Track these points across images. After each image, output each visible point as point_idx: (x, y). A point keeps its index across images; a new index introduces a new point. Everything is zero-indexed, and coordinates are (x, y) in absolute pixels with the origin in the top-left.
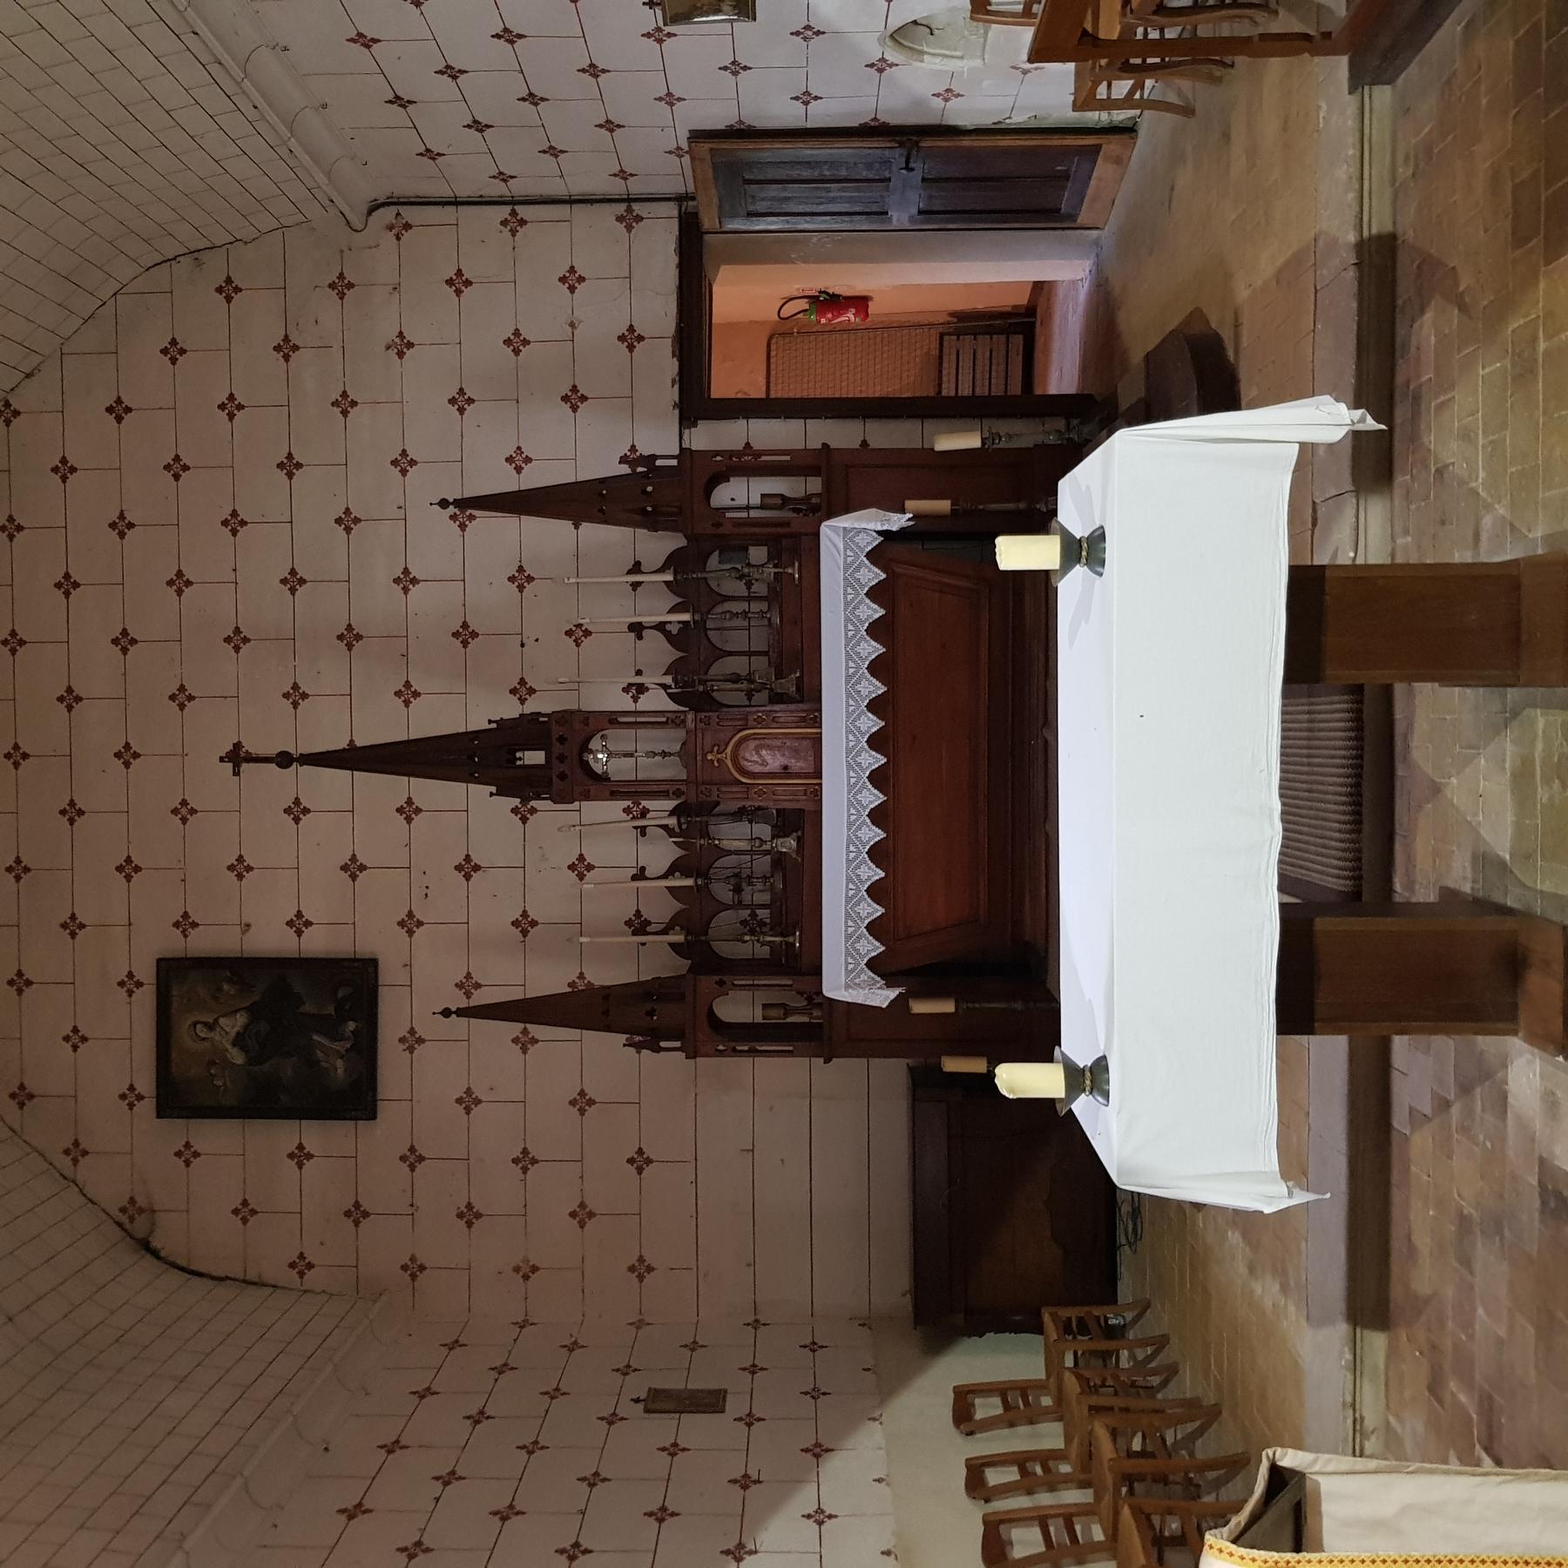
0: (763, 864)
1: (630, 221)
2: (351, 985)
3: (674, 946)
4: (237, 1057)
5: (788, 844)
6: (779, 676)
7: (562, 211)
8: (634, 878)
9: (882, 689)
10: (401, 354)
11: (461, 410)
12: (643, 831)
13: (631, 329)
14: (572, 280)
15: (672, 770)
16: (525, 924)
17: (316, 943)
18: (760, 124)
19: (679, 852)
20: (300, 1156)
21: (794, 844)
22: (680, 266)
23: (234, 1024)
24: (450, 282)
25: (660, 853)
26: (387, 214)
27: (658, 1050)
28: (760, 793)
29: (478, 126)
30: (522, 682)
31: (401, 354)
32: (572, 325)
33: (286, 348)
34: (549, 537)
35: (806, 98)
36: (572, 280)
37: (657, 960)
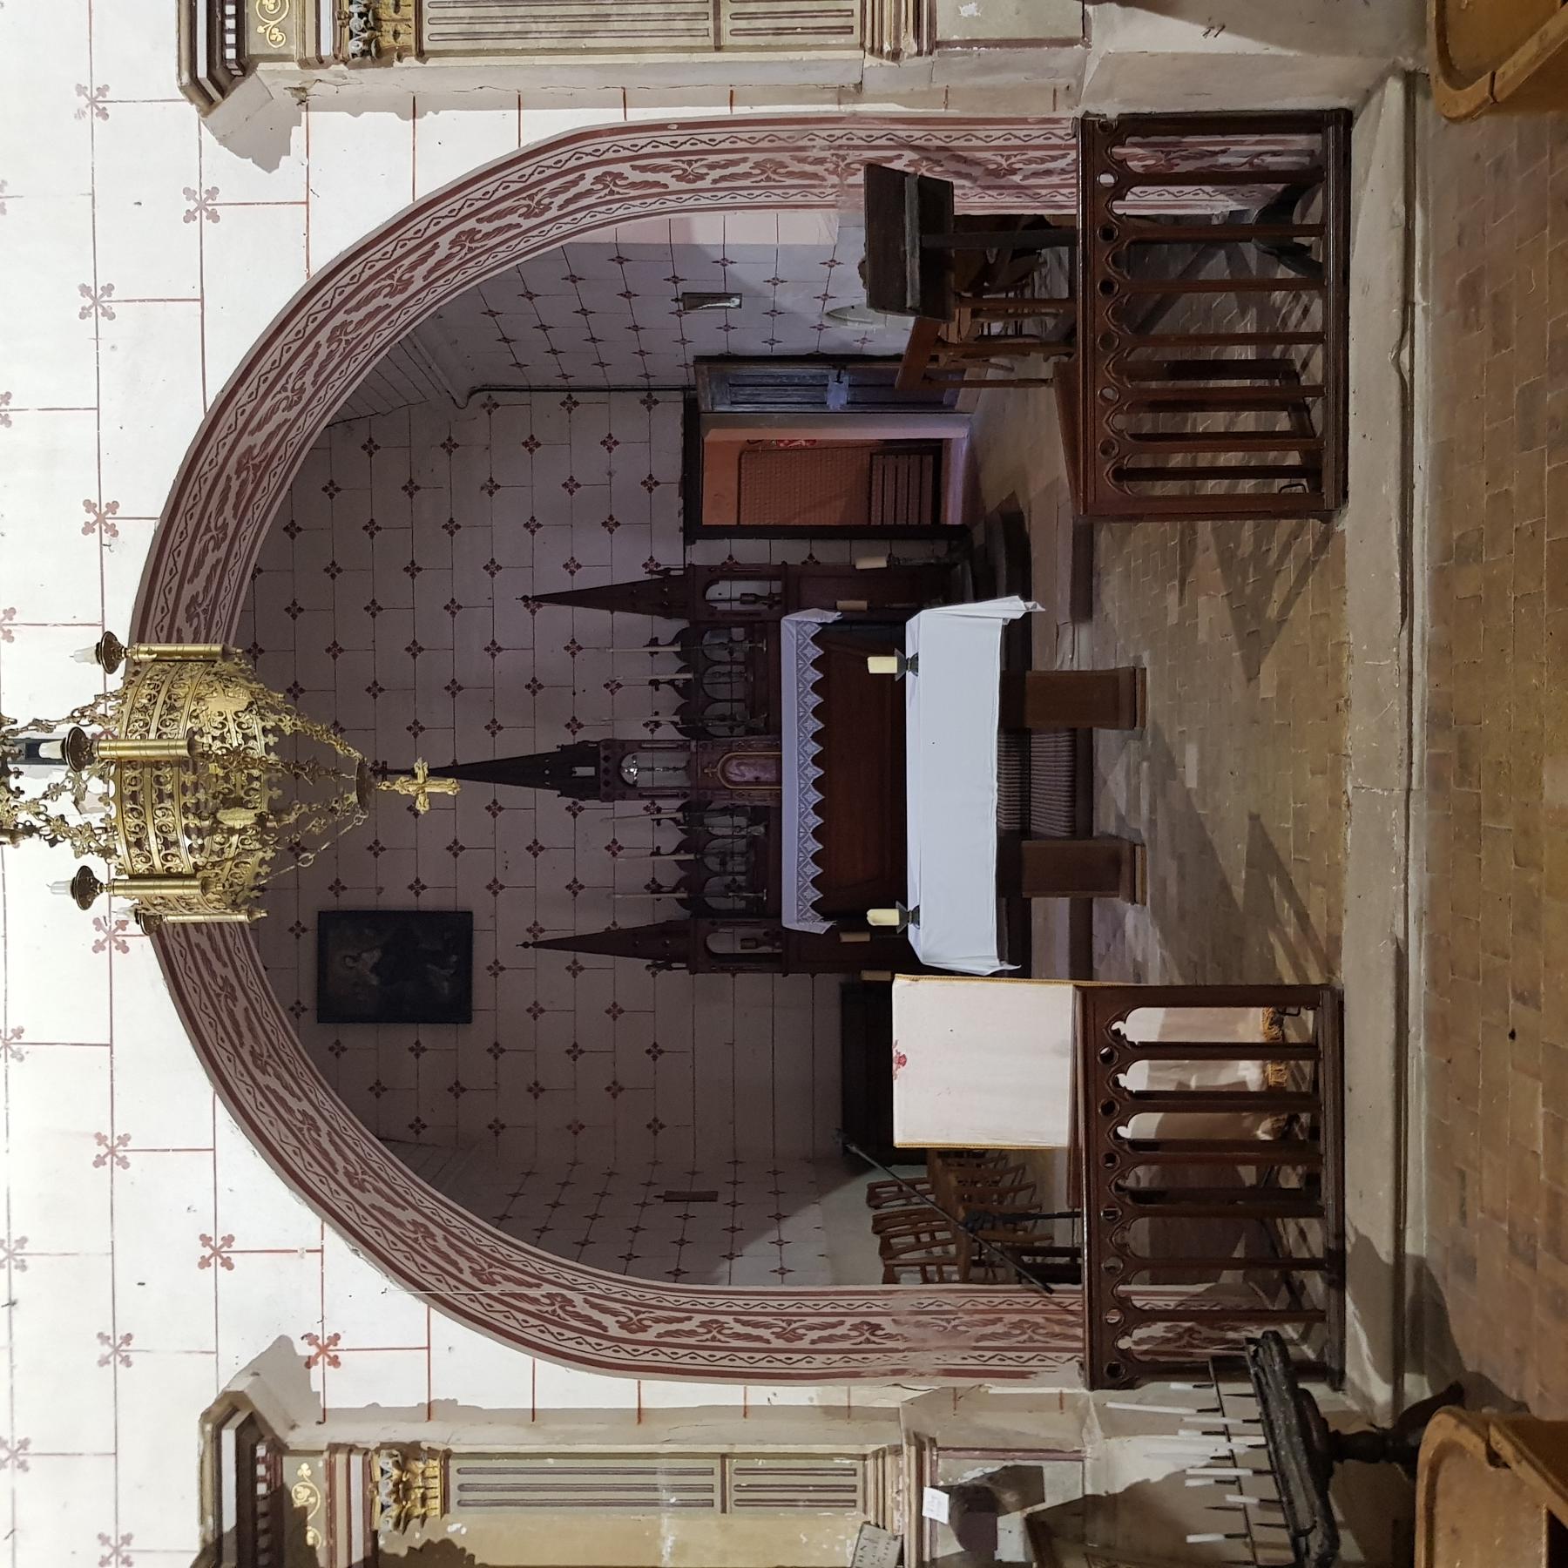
0: (741, 844)
1: (650, 403)
2: (451, 932)
4: (375, 981)
5: (760, 830)
7: (602, 396)
8: (653, 854)
10: (491, 493)
14: (609, 443)
15: (678, 780)
16: (575, 887)
17: (429, 901)
19: (681, 837)
20: (418, 1049)
21: (762, 829)
22: (685, 434)
23: (371, 957)
24: (525, 444)
25: (671, 838)
27: (671, 969)
31: (491, 493)
32: (610, 474)
33: (411, 488)
34: (598, 618)
36: (609, 443)
37: (669, 909)
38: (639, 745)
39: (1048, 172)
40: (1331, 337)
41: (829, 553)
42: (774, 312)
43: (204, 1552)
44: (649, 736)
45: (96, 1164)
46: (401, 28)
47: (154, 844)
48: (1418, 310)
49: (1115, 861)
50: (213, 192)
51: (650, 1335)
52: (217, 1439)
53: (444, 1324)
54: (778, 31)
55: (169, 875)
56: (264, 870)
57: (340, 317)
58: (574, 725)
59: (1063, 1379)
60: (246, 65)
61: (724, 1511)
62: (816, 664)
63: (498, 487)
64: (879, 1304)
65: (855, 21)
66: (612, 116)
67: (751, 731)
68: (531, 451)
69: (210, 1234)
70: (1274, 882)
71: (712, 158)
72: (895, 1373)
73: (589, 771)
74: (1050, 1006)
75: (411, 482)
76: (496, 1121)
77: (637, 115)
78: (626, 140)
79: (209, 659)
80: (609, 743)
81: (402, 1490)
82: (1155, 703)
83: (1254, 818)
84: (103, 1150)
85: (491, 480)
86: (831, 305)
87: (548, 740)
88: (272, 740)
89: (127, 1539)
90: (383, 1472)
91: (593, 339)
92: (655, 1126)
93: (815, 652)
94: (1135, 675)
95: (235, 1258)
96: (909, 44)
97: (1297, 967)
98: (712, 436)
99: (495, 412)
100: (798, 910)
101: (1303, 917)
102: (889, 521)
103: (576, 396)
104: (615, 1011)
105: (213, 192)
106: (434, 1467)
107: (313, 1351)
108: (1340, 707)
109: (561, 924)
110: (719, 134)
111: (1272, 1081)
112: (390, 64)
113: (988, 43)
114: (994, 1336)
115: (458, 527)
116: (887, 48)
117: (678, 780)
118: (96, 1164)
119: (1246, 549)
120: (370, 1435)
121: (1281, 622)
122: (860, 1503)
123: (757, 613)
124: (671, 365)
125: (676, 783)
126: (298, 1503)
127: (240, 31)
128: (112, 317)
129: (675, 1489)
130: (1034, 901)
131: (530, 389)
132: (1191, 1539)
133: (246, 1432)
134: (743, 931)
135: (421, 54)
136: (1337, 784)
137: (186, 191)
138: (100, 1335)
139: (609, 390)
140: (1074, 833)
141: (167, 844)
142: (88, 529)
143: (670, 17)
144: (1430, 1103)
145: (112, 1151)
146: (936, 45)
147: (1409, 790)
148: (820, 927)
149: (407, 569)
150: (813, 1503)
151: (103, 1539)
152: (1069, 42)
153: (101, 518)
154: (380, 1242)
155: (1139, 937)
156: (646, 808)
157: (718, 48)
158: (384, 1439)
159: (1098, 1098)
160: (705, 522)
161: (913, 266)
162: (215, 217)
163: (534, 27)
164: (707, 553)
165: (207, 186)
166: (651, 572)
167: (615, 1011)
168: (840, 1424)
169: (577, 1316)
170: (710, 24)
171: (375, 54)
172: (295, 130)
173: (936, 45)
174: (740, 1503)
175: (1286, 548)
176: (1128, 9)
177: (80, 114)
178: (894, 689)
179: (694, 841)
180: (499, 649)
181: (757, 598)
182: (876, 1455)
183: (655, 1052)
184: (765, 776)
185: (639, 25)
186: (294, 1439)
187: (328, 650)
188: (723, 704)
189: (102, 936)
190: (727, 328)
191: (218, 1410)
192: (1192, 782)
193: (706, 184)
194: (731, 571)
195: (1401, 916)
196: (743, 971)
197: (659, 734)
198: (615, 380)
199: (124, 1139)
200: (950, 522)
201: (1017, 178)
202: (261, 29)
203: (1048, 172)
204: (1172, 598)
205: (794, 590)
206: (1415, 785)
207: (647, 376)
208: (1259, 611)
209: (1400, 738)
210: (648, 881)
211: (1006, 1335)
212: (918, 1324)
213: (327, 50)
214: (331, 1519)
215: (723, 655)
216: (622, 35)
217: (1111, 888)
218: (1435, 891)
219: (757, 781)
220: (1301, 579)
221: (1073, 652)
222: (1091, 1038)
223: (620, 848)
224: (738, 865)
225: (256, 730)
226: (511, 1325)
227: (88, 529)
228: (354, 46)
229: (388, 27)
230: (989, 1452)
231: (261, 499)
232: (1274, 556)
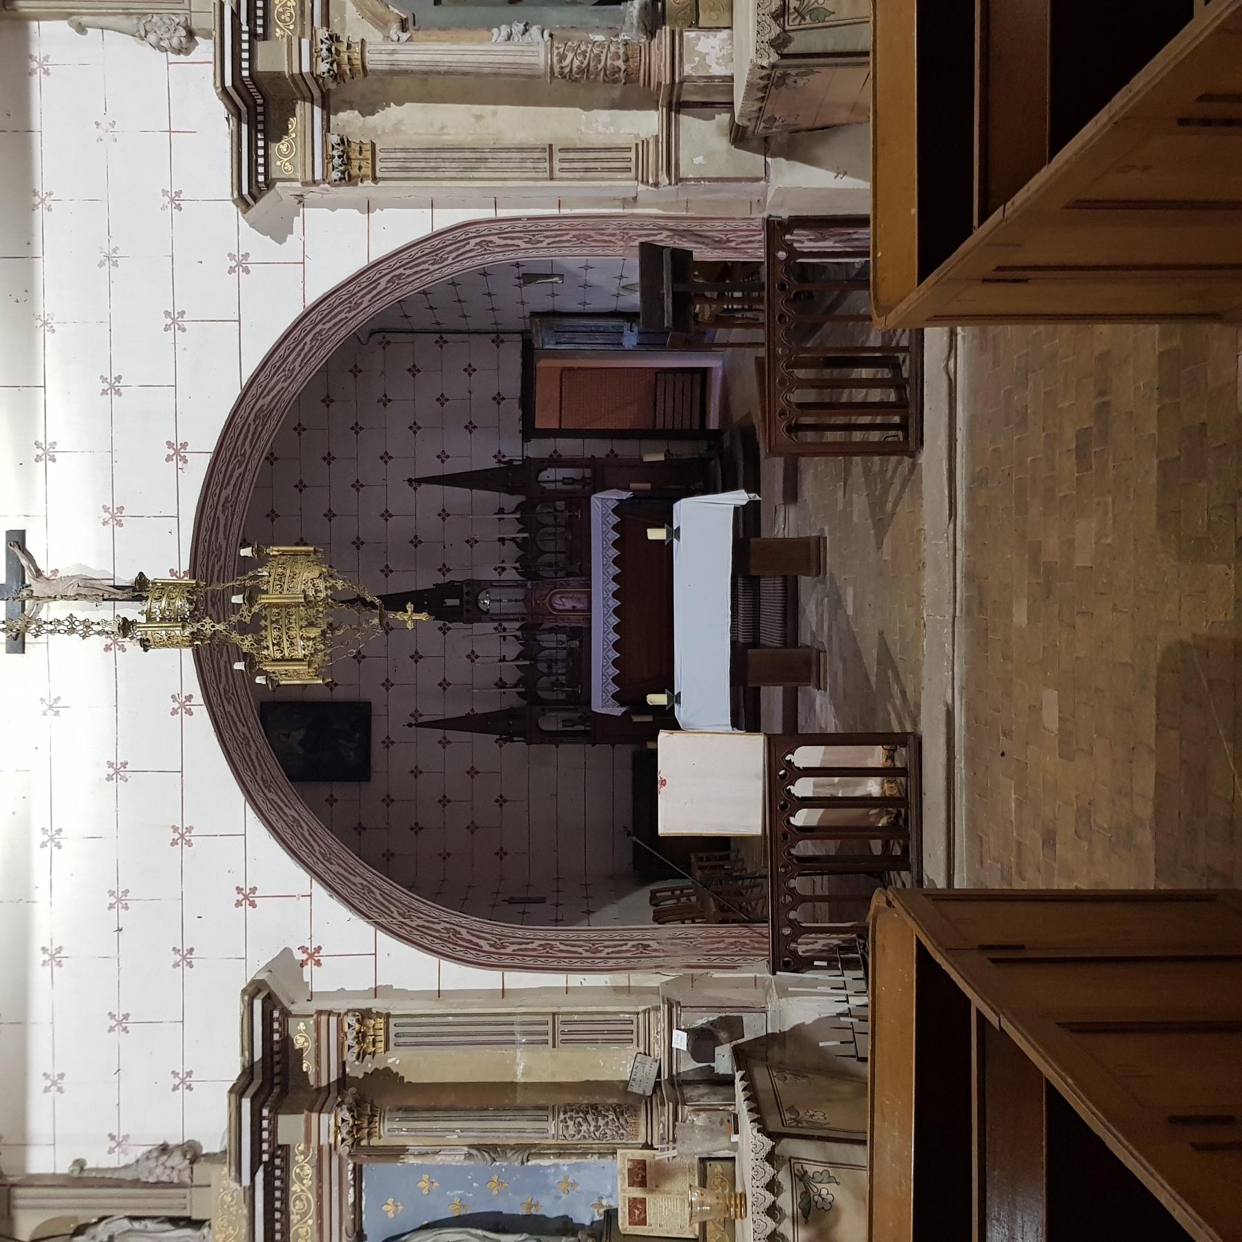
1: (498, 342)
3: (518, 693)
4: (300, 751)
6: (571, 564)
8: (500, 661)
10: (385, 405)
12: (504, 638)
14: (470, 370)
15: (519, 608)
16: (444, 685)
19: (520, 648)
22: (523, 364)
23: (298, 735)
26: (379, 337)
28: (563, 620)
30: (444, 565)
31: (385, 405)
34: (459, 495)
36: (470, 370)
37: (511, 699)
38: (491, 584)
39: (751, 242)
40: (913, 349)
41: (625, 449)
42: (585, 286)
43: (243, 1073)
44: (498, 578)
46: (363, 164)
47: (286, 644)
48: (959, 338)
49: (807, 663)
50: (246, 256)
51: (509, 950)
52: (251, 1005)
53: (383, 937)
54: (587, 170)
55: (292, 660)
56: (327, 658)
57: (320, 327)
58: (444, 569)
59: (758, 970)
60: (269, 184)
61: (554, 1046)
62: (615, 528)
64: (650, 934)
65: (632, 165)
66: (489, 213)
67: (569, 575)
69: (242, 886)
70: (890, 672)
71: (546, 233)
72: (656, 967)
73: (456, 602)
74: (753, 747)
75: (328, 396)
76: (388, 851)
77: (503, 213)
78: (497, 226)
79: (307, 554)
80: (470, 582)
81: (361, 1037)
82: (831, 560)
83: (881, 634)
84: (177, 836)
85: (385, 396)
86: (624, 282)
87: (427, 580)
88: (329, 592)
89: (190, 1074)
90: (350, 1026)
91: (459, 301)
92: (501, 854)
93: (615, 519)
94: (820, 541)
95: (257, 901)
96: (663, 178)
97: (901, 723)
98: (542, 364)
99: (388, 348)
100: (603, 701)
101: (903, 693)
102: (669, 426)
104: (473, 772)
105: (246, 256)
106: (380, 1023)
107: (305, 957)
108: (921, 566)
109: (435, 709)
110: (552, 223)
111: (888, 793)
112: (356, 184)
113: (710, 180)
114: (718, 949)
115: (361, 428)
116: (651, 181)
117: (519, 608)
119: (876, 468)
120: (341, 1006)
121: (893, 515)
122: (635, 1041)
123: (574, 492)
124: (513, 317)
125: (517, 611)
126: (297, 1047)
127: (266, 165)
128: (184, 330)
129: (524, 1033)
130: (764, 689)
131: (413, 332)
132: (821, 1044)
133: (267, 1002)
134: (566, 715)
135: (375, 179)
136: (919, 613)
137: (230, 255)
138: (174, 949)
139: (469, 332)
140: (785, 644)
141: (292, 644)
142: (169, 459)
143: (523, 160)
144: (967, 800)
145: (182, 836)
146: (679, 180)
147: (954, 617)
148: (618, 711)
149: (324, 459)
151: (175, 1074)
152: (757, 180)
153: (177, 452)
154: (345, 892)
155: (822, 710)
156: (496, 629)
157: (552, 179)
158: (350, 1007)
159: (779, 800)
160: (537, 426)
161: (668, 302)
162: (247, 271)
163: (442, 165)
164: (539, 449)
165: (242, 252)
166: (499, 461)
167: (473, 772)
168: (623, 997)
169: (464, 940)
170: (547, 165)
171: (348, 179)
172: (296, 219)
173: (679, 180)
174: (564, 1042)
175: (896, 469)
176: (792, 162)
177: (164, 208)
178: (665, 551)
179: (529, 652)
180: (391, 516)
181: (573, 481)
182: (644, 1012)
183: (501, 801)
184: (579, 606)
185: (505, 165)
186: (294, 1009)
187: (268, 516)
188: (549, 549)
189: (176, 705)
190: (553, 295)
191: (250, 990)
192: (850, 612)
193: (544, 244)
194: (556, 461)
195: (949, 691)
196: (563, 742)
197: (504, 576)
198: (473, 326)
199: (190, 829)
200: (711, 427)
201: (733, 244)
202: (279, 163)
203: (751, 242)
204: (840, 493)
205: (600, 475)
206: (958, 614)
207: (496, 324)
208: (882, 506)
209: (948, 586)
210: (497, 680)
211: (725, 949)
212: (672, 944)
213: (318, 176)
214: (318, 1056)
215: (550, 520)
216: (494, 169)
217: (807, 681)
218: (968, 675)
219: (574, 609)
220: (903, 489)
221: (784, 525)
222: (773, 763)
223: (477, 657)
224: (560, 668)
225: (322, 587)
226: (425, 942)
227: (169, 459)
228: (335, 175)
229: (355, 163)
230: (710, 1008)
231: (265, 435)
232: (889, 474)
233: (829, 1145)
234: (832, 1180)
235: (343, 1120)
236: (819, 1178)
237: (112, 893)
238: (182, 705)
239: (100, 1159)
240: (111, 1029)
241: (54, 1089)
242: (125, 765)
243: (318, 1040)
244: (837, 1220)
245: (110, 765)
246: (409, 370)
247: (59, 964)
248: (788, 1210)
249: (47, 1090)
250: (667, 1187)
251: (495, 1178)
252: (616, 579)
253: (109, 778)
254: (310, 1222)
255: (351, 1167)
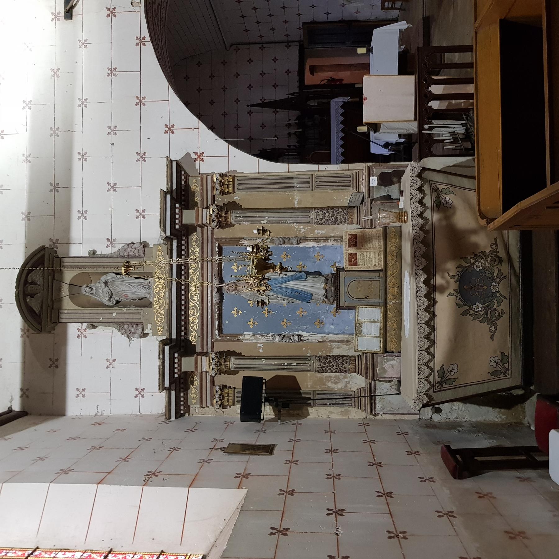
1: (288, 47)
7: (273, 45)
9: (344, 135)
10: (237, 77)
11: (250, 89)
13: (288, 70)
14: (275, 60)
18: (318, 20)
22: (299, 56)
26: (234, 47)
29: (258, 23)
33: (212, 77)
35: (328, 13)
36: (275, 60)
45: (136, 105)
53: (233, 149)
61: (312, 189)
62: (342, 115)
63: (239, 75)
68: (250, 63)
74: (410, 81)
84: (138, 101)
89: (144, 211)
93: (342, 111)
103: (265, 45)
107: (196, 157)
118: (136, 105)
122: (352, 186)
131: (250, 44)
145: (141, 101)
150: (338, 186)
174: (317, 186)
189: (138, 41)
199: (144, 98)
233: (450, 176)
234: (451, 193)
235: (213, 211)
236: (444, 191)
237: (109, 128)
238: (141, 41)
239: (102, 250)
240: (109, 190)
241: (82, 217)
242: (115, 69)
243: (202, 186)
244: (454, 213)
245: (109, 69)
246: (248, 61)
247: (86, 160)
248: (429, 205)
249: (79, 218)
250: (367, 246)
251: (285, 320)
252: (342, 139)
253: (108, 75)
254: (198, 273)
255: (217, 245)
